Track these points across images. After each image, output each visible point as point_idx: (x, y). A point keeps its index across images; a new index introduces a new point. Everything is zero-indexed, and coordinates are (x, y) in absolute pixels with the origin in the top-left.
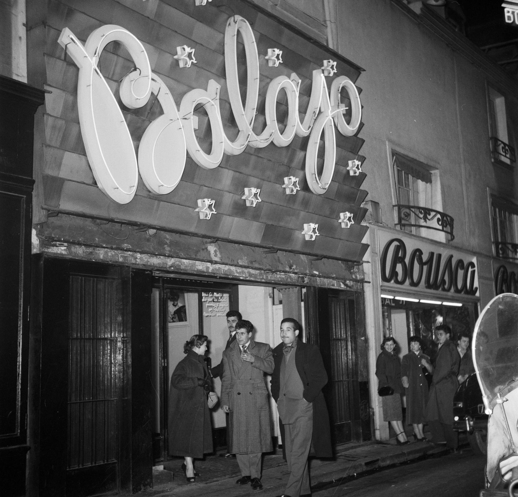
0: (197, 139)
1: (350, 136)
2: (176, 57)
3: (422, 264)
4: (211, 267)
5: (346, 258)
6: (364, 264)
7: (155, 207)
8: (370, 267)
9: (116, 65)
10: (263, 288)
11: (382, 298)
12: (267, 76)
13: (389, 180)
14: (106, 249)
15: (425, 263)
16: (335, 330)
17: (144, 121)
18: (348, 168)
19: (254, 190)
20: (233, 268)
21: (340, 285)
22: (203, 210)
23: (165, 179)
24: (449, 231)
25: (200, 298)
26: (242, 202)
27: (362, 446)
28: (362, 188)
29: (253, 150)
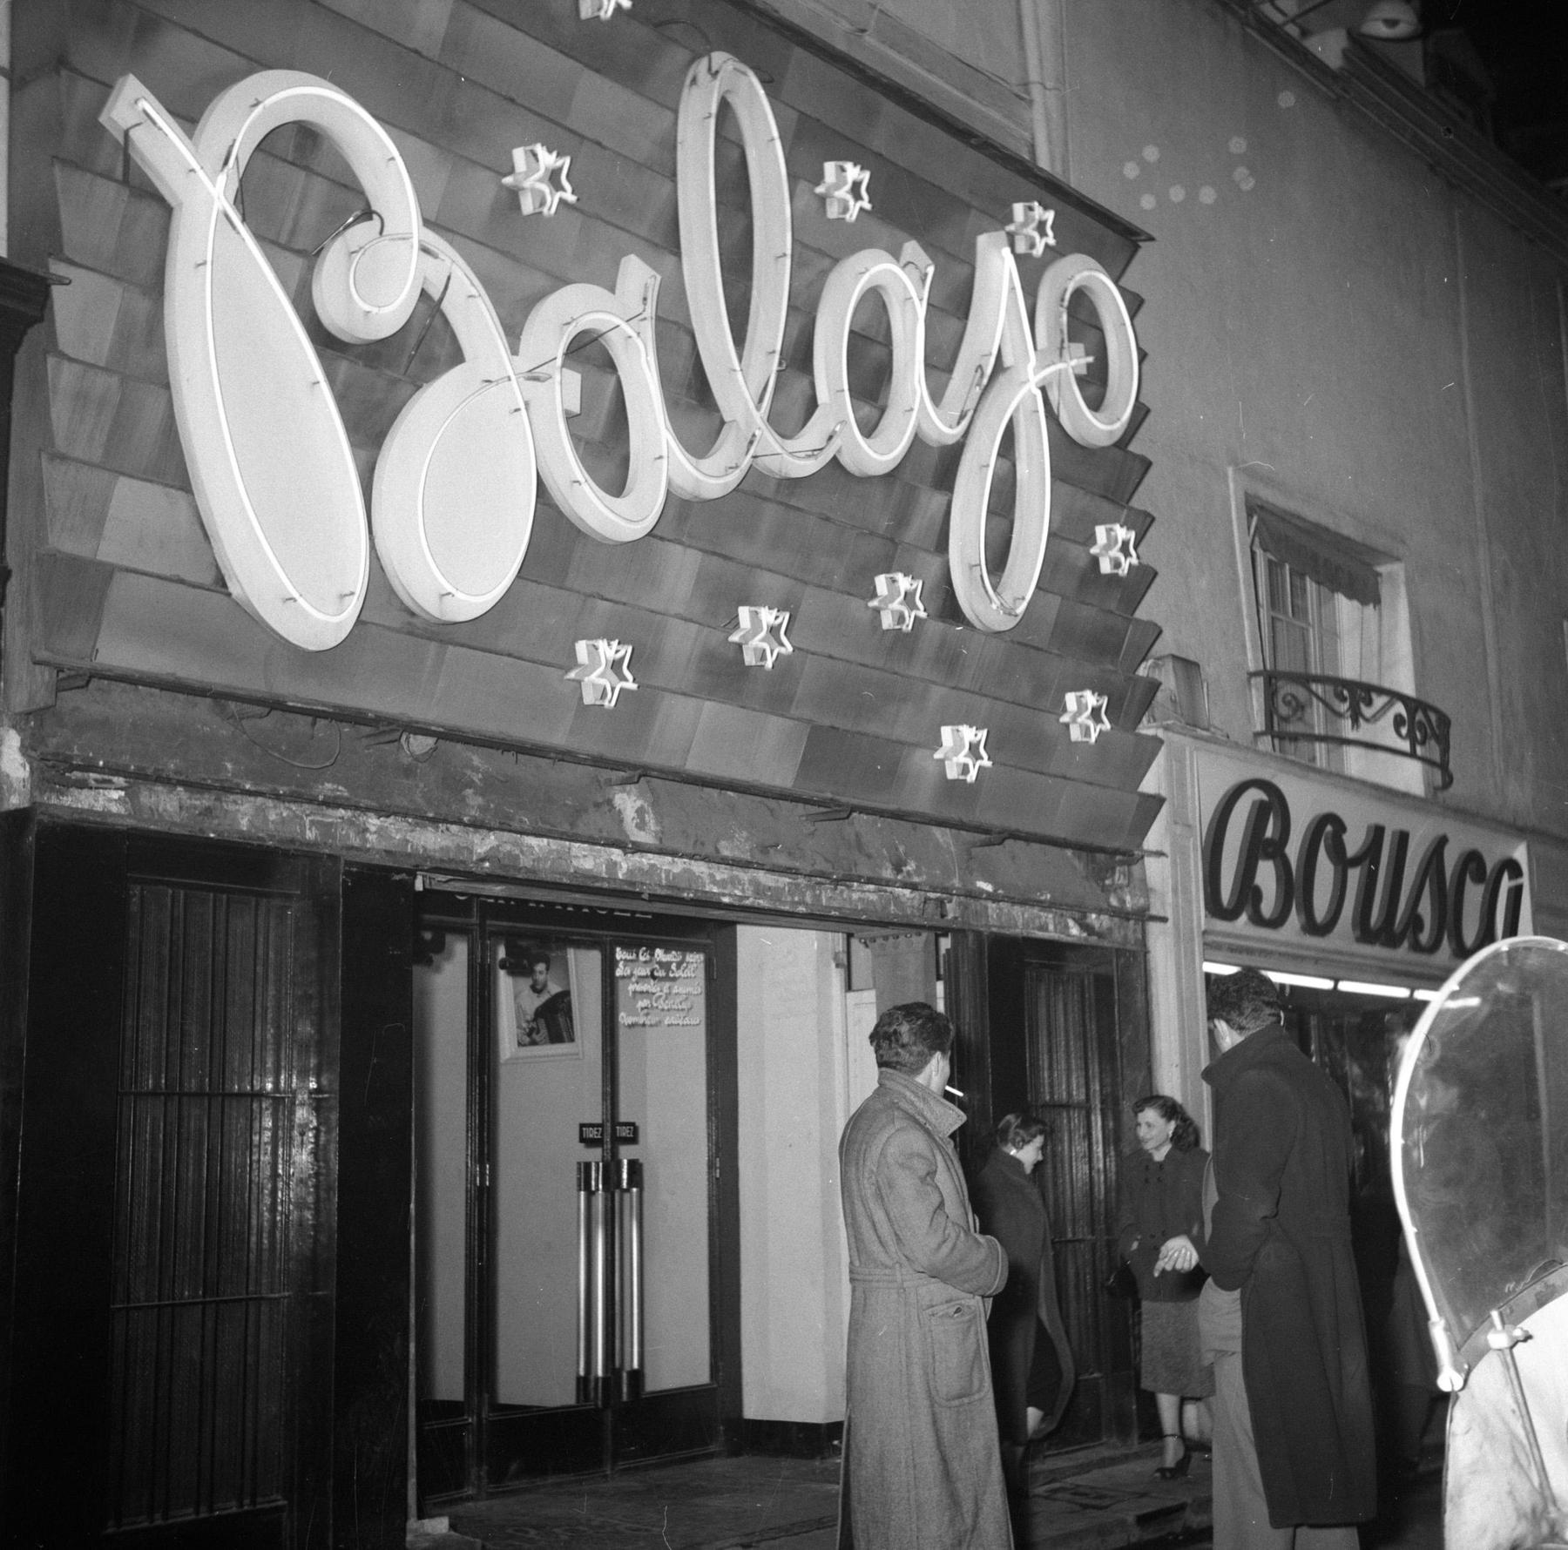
0: (576, 448)
1: (1103, 448)
2: (508, 180)
3: (1342, 862)
4: (624, 864)
5: (1088, 840)
6: (1147, 860)
7: (429, 663)
8: (1166, 869)
9: (302, 204)
10: (813, 934)
11: (1208, 976)
12: (818, 252)
13: (1237, 592)
14: (260, 800)
15: (1355, 862)
16: (1051, 1076)
17: (394, 382)
18: (1094, 551)
19: (768, 616)
20: (700, 868)
21: (1067, 927)
22: (594, 677)
23: (465, 570)
24: (1437, 757)
25: (609, 965)
26: (731, 654)
27: (1137, 1456)
28: (1141, 613)
29: (773, 486)
